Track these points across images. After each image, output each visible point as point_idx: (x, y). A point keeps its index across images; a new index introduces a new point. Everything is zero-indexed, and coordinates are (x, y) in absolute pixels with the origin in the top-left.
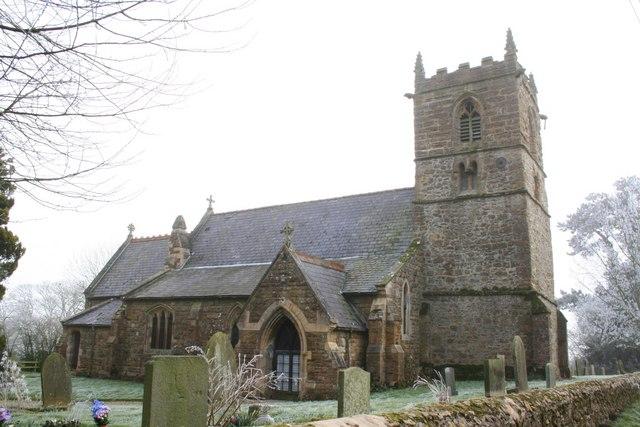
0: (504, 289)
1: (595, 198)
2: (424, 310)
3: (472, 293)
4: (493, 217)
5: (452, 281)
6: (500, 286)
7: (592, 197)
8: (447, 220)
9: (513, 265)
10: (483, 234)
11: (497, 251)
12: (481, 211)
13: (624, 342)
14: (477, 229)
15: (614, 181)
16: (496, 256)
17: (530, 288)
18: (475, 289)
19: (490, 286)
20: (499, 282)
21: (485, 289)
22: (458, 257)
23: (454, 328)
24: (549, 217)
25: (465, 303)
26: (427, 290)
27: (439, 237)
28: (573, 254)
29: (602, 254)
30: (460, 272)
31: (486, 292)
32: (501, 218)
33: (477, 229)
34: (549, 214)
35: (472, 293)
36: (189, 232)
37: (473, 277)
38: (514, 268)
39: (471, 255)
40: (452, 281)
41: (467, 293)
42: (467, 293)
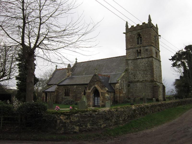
9: (150, 75)
11: (146, 71)
16: (146, 73)
23: (136, 90)
24: (161, 61)
25: (138, 84)
26: (129, 81)
27: (132, 68)
29: (182, 69)
32: (147, 63)
34: (161, 61)
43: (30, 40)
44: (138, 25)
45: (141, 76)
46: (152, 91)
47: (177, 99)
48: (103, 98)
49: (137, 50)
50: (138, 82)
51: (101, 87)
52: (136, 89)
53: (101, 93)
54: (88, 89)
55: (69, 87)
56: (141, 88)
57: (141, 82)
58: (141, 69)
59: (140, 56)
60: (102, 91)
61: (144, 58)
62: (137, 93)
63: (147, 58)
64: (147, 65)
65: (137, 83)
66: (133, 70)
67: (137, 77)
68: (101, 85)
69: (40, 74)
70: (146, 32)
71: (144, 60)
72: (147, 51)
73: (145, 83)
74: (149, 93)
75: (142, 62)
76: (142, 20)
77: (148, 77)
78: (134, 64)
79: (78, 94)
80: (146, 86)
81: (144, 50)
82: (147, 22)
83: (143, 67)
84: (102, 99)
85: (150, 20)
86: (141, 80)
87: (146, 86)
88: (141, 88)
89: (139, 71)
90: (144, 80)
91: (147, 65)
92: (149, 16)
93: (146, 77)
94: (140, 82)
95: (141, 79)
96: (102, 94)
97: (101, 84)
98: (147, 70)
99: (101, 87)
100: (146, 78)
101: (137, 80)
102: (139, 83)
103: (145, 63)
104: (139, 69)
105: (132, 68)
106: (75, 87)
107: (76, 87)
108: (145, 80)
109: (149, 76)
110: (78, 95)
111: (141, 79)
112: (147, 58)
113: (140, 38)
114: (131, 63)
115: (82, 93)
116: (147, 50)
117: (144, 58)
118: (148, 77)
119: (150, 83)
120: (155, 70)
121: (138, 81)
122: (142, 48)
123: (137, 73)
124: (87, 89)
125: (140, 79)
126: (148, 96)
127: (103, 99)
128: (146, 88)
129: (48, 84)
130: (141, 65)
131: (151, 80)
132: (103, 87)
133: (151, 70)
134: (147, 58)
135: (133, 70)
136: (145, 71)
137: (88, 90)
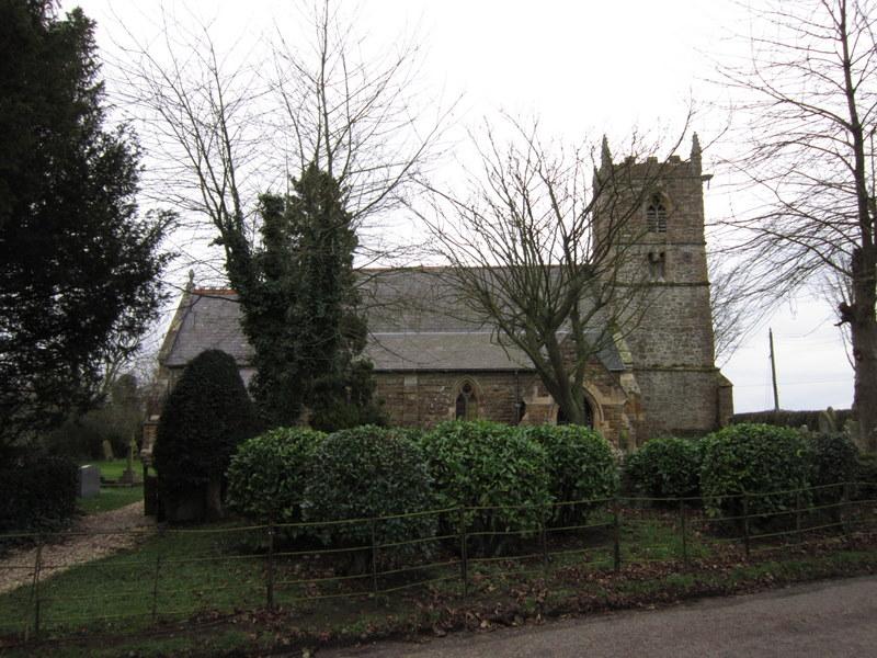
32: (688, 305)
43: (844, 79)
44: (652, 161)
45: (669, 348)
46: (708, 404)
48: (611, 427)
49: (650, 255)
50: (656, 370)
51: (601, 383)
53: (605, 407)
54: (539, 390)
55: (476, 382)
56: (670, 392)
57: (670, 370)
58: (668, 325)
59: (663, 275)
60: (607, 401)
61: (678, 285)
62: (653, 411)
63: (690, 285)
64: (687, 310)
65: (652, 373)
68: (603, 376)
70: (683, 192)
71: (677, 290)
72: (689, 262)
73: (686, 374)
74: (698, 411)
75: (670, 297)
76: (662, 145)
79: (427, 416)
80: (687, 385)
81: (678, 257)
82: (684, 154)
83: (673, 318)
84: (608, 430)
85: (696, 153)
86: (667, 364)
87: (687, 385)
88: (670, 392)
89: (660, 331)
90: (678, 363)
91: (687, 310)
92: (605, 140)
93: (688, 353)
94: (665, 371)
96: (608, 410)
97: (601, 374)
98: (691, 329)
99: (601, 383)
100: (686, 359)
101: (653, 363)
102: (659, 374)
103: (680, 304)
104: (658, 325)
106: (410, 381)
107: (419, 386)
108: (683, 365)
110: (427, 420)
112: (689, 289)
113: (659, 209)
115: (447, 411)
116: (687, 257)
117: (678, 285)
118: (692, 354)
119: (704, 376)
121: (656, 365)
122: (669, 247)
123: (650, 336)
124: (533, 392)
126: (696, 420)
127: (610, 433)
128: (689, 391)
129: (169, 363)
131: (704, 366)
132: (609, 385)
133: (703, 328)
134: (690, 285)
136: (683, 331)
137: (539, 396)
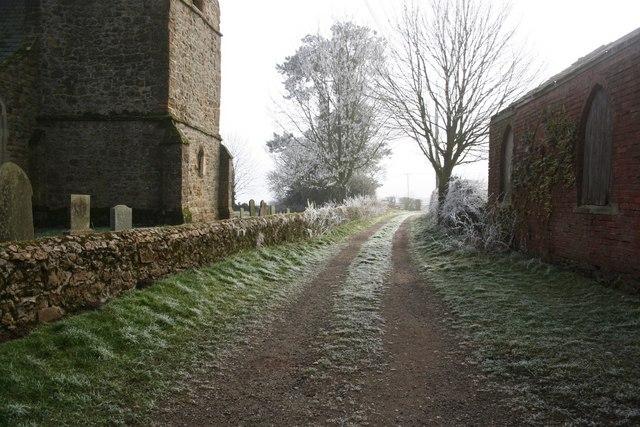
0: (136, 113)
1: (310, 40)
2: (36, 138)
3: (96, 118)
4: (127, 20)
5: (75, 101)
6: (131, 110)
7: (309, 39)
8: (70, 21)
9: (148, 84)
10: (114, 42)
11: (129, 65)
12: (113, 10)
13: (314, 184)
14: (107, 36)
15: (331, 25)
16: (129, 71)
17: (166, 111)
18: (102, 112)
19: (119, 109)
20: (130, 104)
21: (113, 113)
22: (83, 71)
23: (74, 162)
24: (220, 35)
25: (88, 131)
26: (42, 113)
27: (58, 42)
28: (289, 97)
29: (314, 102)
30: (82, 91)
31: (114, 117)
32: (138, 21)
33: (107, 36)
34: (221, 31)
35: (96, 118)
36: (486, 200)
37: (100, 98)
38: (149, 88)
39: (98, 69)
40: (75, 101)
41: (93, 117)
42: (93, 117)
47: (401, 199)
52: (75, 157)
66: (64, 52)
67: (78, 86)
69: (363, 218)
77: (138, 95)
78: (70, 21)
83: (114, 42)
95: (105, 102)
105: (58, 42)
109: (143, 88)
111: (105, 102)
114: (54, 13)
118: (138, 95)
120: (182, 61)
125: (98, 102)
130: (107, 31)
135: (64, 52)
